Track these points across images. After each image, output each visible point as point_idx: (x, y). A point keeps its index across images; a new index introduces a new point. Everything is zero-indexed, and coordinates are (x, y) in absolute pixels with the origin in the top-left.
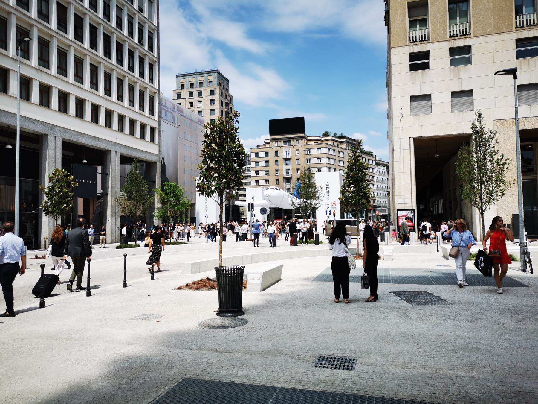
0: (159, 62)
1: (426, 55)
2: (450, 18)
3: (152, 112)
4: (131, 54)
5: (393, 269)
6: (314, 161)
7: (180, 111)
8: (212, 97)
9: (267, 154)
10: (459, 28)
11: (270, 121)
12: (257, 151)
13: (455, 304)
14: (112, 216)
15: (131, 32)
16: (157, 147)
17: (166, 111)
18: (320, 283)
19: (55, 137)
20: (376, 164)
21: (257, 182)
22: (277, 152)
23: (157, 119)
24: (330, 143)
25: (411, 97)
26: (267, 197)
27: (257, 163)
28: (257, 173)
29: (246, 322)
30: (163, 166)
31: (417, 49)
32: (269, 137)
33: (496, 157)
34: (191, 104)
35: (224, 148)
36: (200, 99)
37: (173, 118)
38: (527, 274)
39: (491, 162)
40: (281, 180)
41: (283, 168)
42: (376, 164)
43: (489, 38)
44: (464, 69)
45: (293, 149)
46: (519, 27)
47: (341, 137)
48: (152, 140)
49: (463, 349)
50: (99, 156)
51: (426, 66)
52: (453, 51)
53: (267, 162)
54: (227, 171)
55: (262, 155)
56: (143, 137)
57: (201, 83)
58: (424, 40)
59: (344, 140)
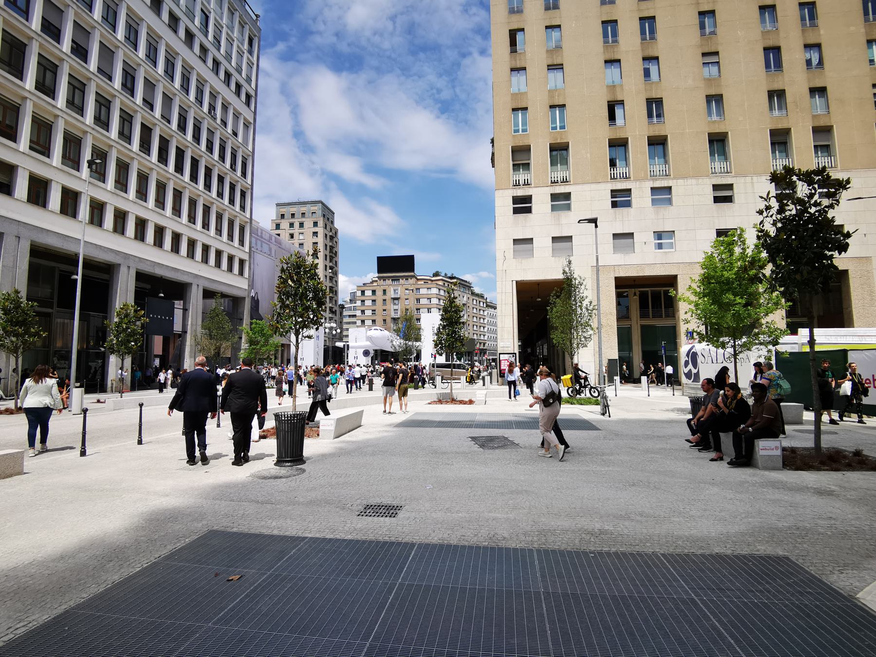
0: (252, 189)
1: (528, 199)
2: (552, 165)
3: (242, 242)
4: (221, 179)
5: (481, 414)
6: (423, 301)
7: (279, 243)
8: (316, 229)
9: (374, 292)
10: (560, 174)
11: (379, 258)
12: (363, 289)
13: (525, 447)
14: (191, 357)
15: (222, 157)
16: (246, 282)
17: (262, 242)
18: (406, 429)
19: (129, 267)
20: (487, 306)
21: (363, 322)
22: (384, 291)
23: (247, 250)
24: (441, 283)
25: (514, 240)
26: (369, 339)
27: (363, 301)
28: (363, 312)
29: (304, 471)
30: (255, 303)
31: (520, 192)
32: (377, 275)
33: (585, 303)
34: (292, 236)
35: (301, 285)
36: (301, 231)
37: (270, 250)
38: (606, 418)
39: (580, 306)
40: (389, 320)
41: (391, 307)
42: (487, 306)
43: (587, 187)
44: (564, 215)
45: (399, 288)
46: (613, 178)
47: (451, 278)
48: (241, 273)
49: (512, 492)
50: (178, 290)
51: (528, 210)
52: (554, 197)
53: (374, 301)
54: (303, 310)
55: (368, 293)
56: (230, 269)
57: (293, 215)
58: (527, 184)
59: (455, 280)
